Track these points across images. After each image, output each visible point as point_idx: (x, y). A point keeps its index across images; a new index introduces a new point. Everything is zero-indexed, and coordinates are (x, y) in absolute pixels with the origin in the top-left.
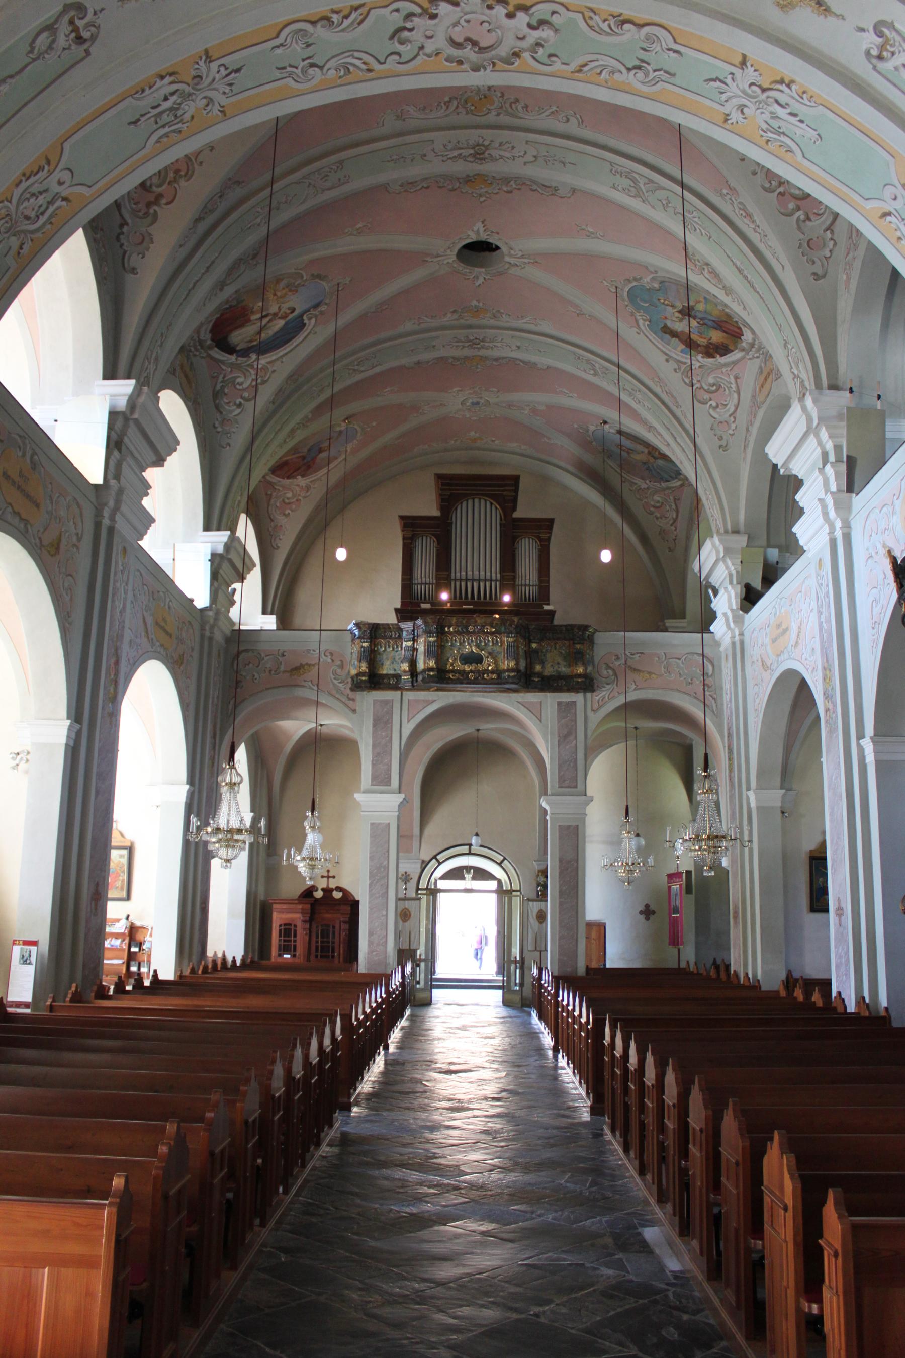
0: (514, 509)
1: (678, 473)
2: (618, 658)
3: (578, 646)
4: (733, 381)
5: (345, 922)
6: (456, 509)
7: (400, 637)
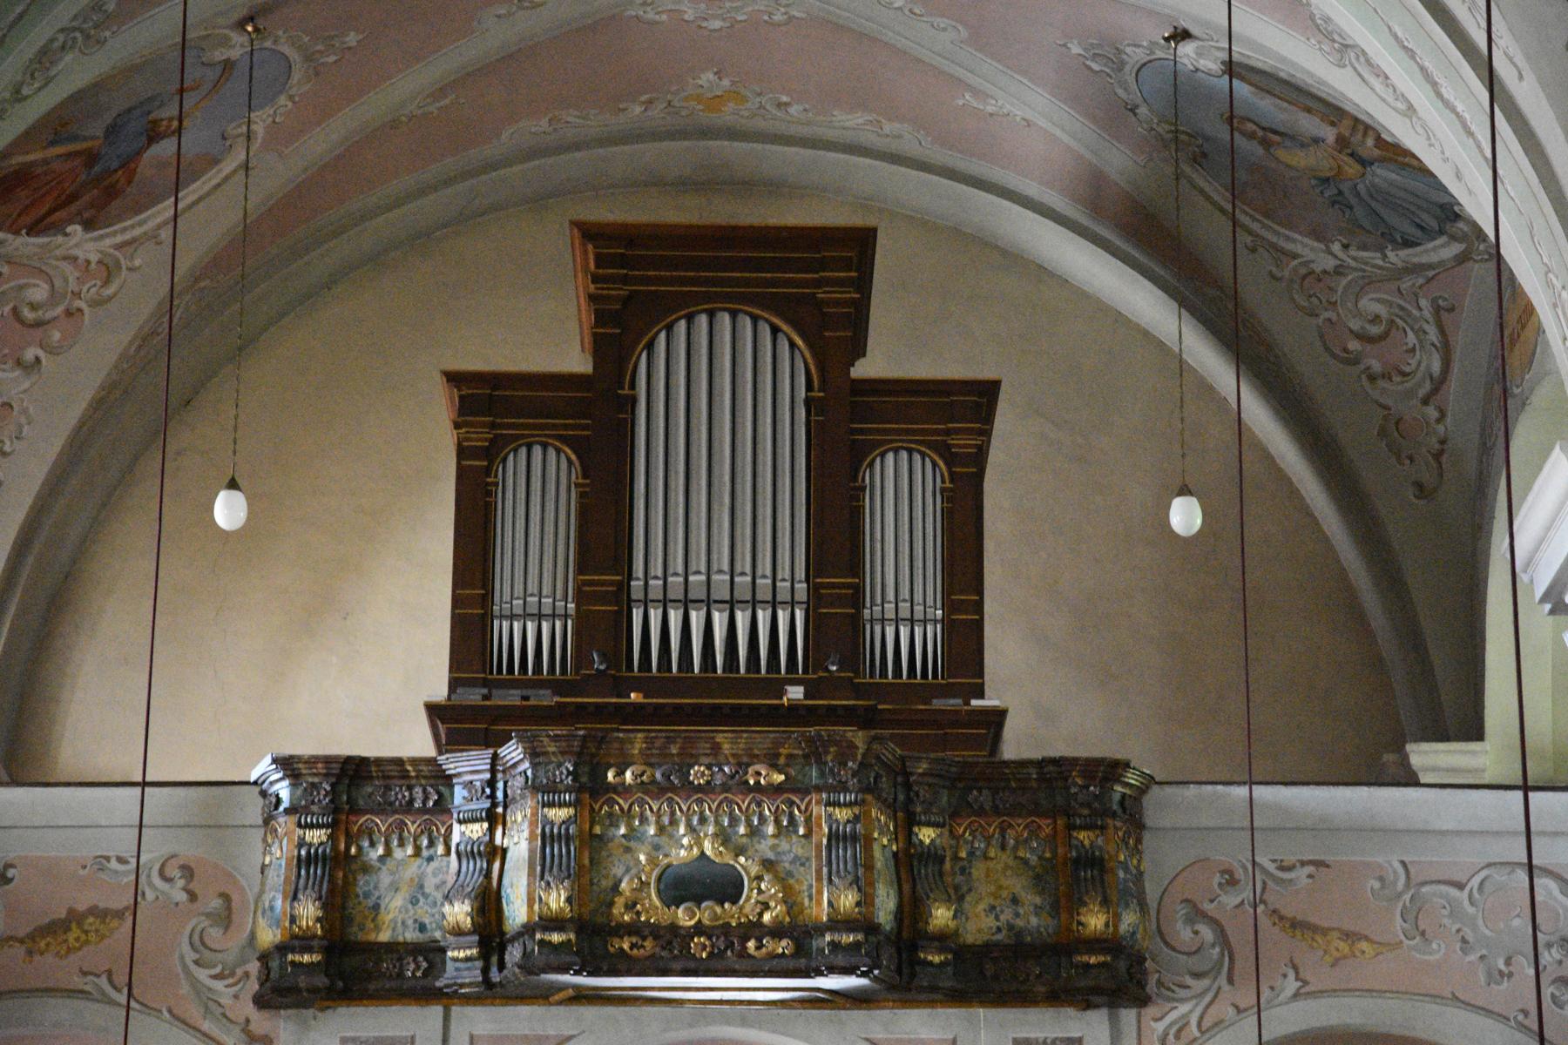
0: (858, 348)
1: (1449, 214)
3: (1084, 836)
7: (442, 807)
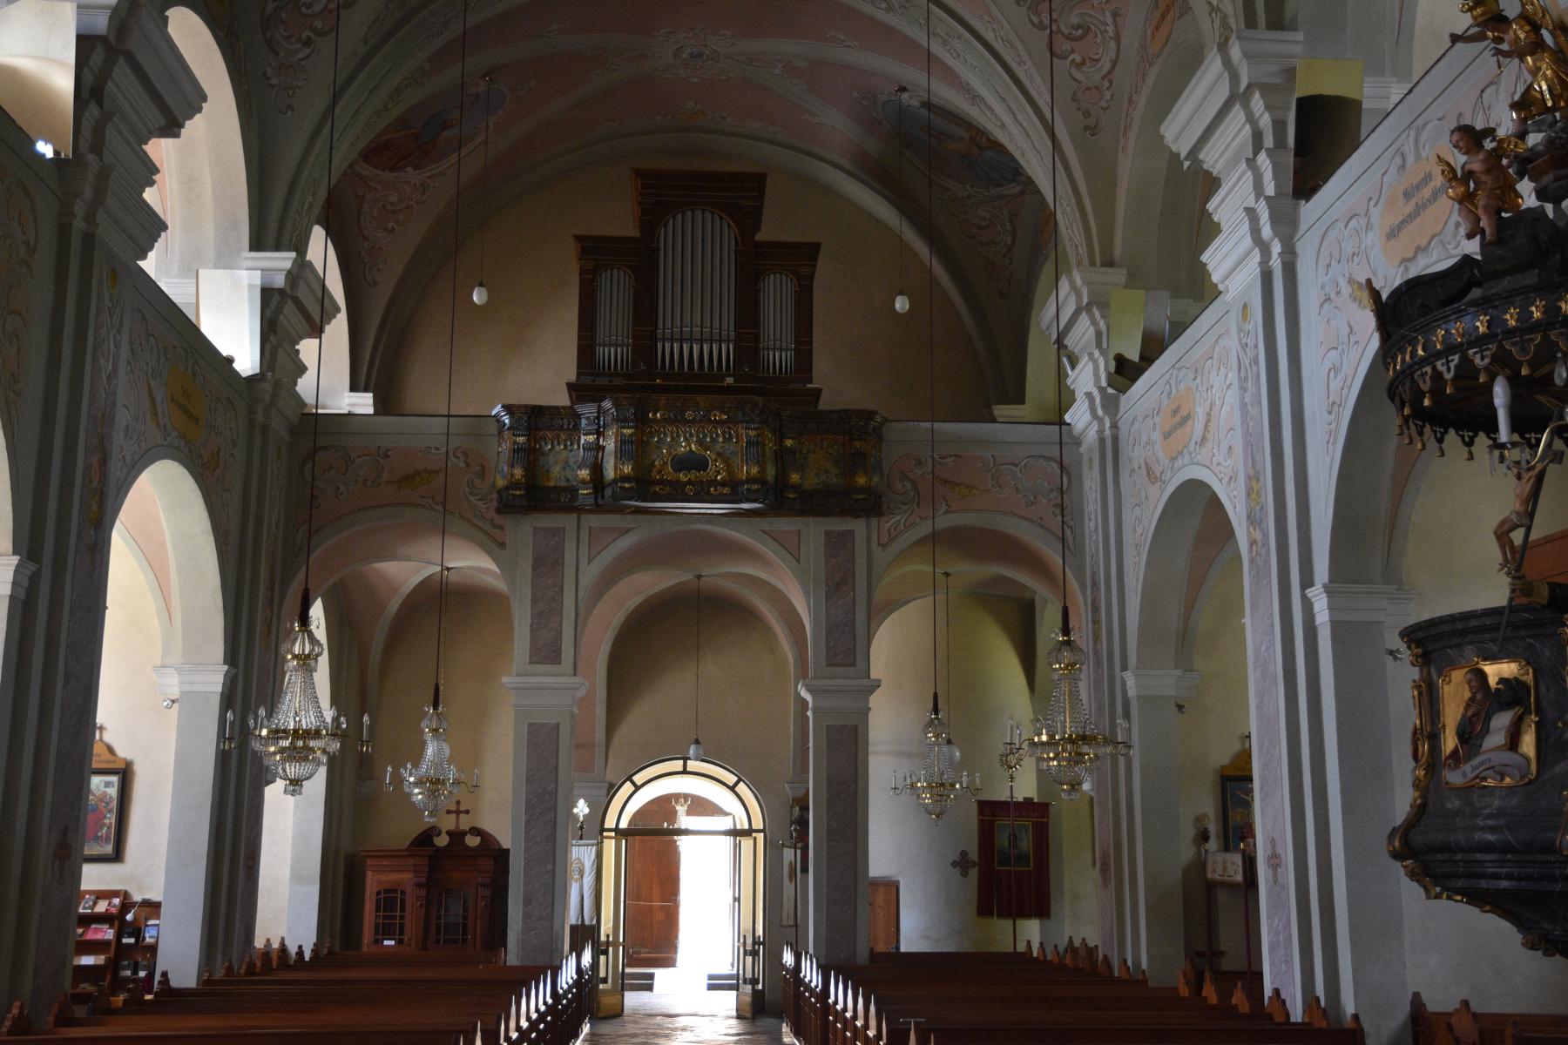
2: (920, 463)
3: (857, 443)
4: (1109, 20)
5: (485, 885)
6: (666, 226)
7: (577, 428)
